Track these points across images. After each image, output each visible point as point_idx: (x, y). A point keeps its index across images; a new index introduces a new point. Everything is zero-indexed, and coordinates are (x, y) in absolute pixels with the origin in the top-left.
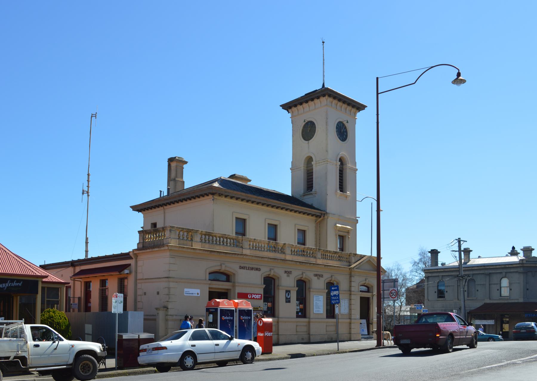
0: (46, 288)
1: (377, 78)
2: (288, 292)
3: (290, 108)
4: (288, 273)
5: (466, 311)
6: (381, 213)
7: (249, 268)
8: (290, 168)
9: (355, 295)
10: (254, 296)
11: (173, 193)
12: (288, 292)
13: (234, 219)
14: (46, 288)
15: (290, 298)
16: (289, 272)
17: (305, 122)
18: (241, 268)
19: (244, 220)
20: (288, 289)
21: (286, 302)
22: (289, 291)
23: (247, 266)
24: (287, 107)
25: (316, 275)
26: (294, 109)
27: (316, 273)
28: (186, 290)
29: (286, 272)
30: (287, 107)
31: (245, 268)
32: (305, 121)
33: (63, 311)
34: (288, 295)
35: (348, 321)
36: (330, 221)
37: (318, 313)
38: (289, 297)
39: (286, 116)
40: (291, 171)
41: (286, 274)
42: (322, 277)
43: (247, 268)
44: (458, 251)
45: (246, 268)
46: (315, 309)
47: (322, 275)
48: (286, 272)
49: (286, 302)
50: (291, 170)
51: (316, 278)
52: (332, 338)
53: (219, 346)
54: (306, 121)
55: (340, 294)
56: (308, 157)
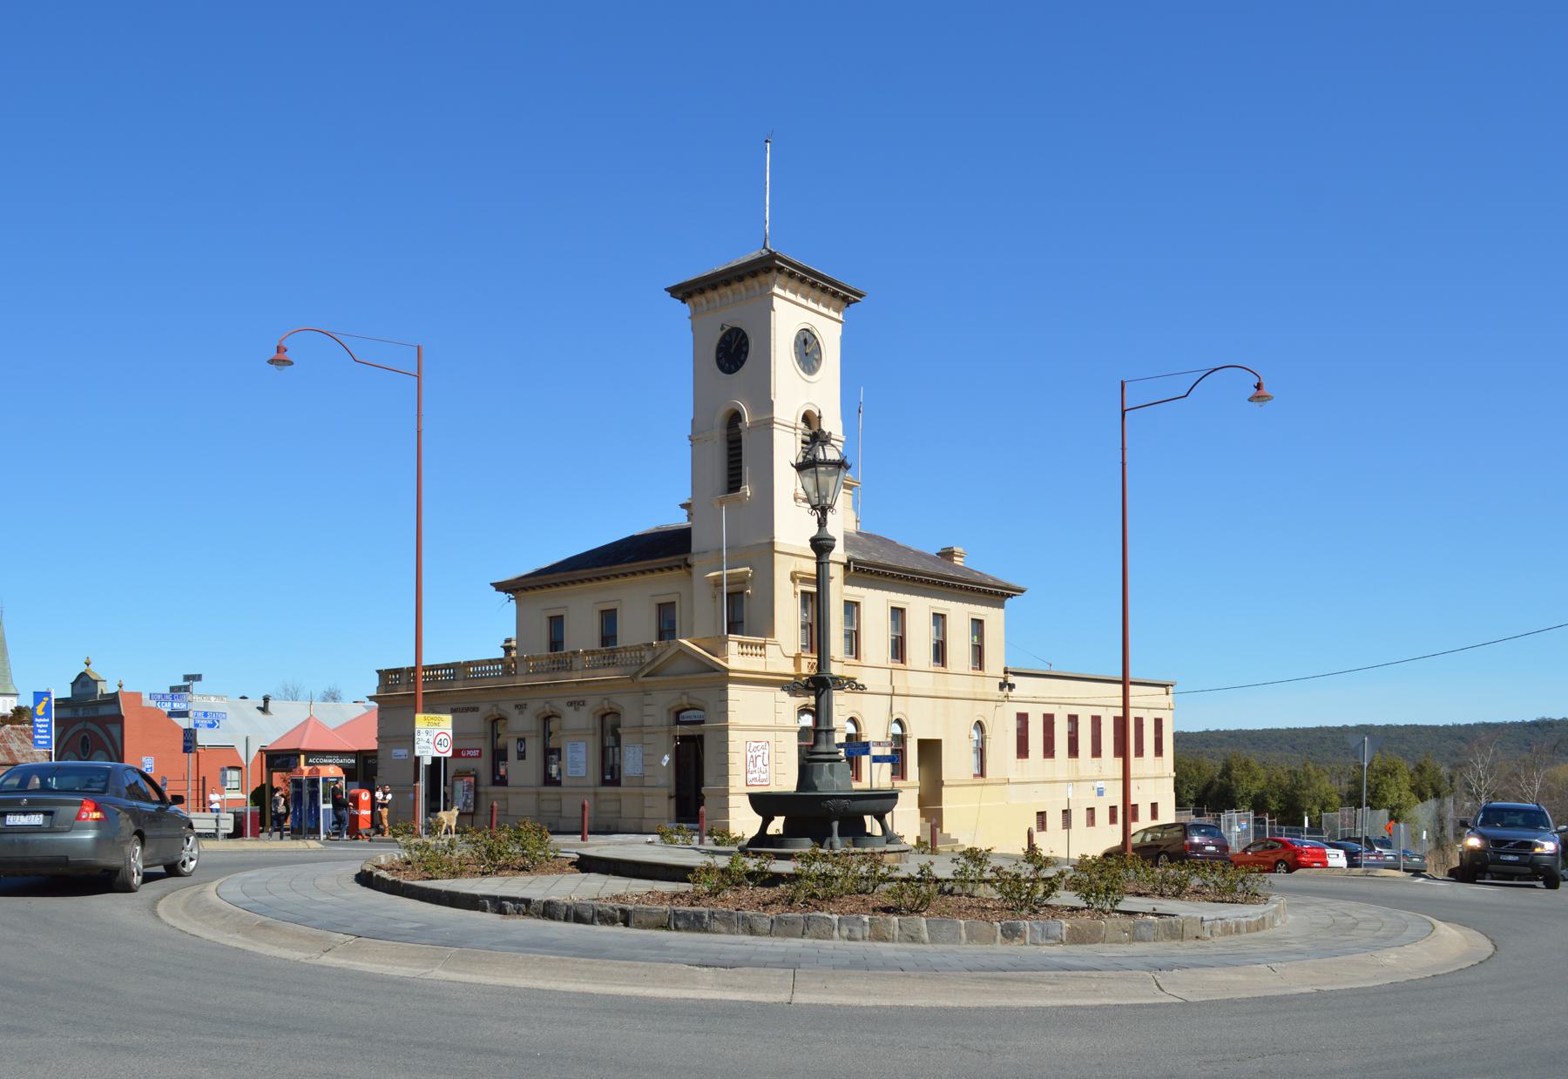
1: (1122, 382)
2: (521, 741)
4: (521, 707)
6: (1126, 452)
8: (690, 436)
9: (654, 733)
10: (469, 753)
11: (689, 673)
12: (521, 741)
13: (890, 609)
15: (524, 751)
17: (724, 331)
19: (902, 610)
20: (521, 736)
21: (519, 759)
23: (464, 705)
24: (683, 292)
25: (570, 704)
26: (698, 299)
27: (571, 699)
28: (394, 751)
29: (516, 706)
30: (683, 292)
32: (722, 329)
34: (521, 746)
35: (977, 805)
39: (683, 309)
40: (690, 442)
41: (517, 711)
46: (569, 769)
47: (583, 702)
48: (516, 706)
49: (519, 759)
50: (692, 441)
52: (609, 827)
53: (449, 708)
54: (727, 328)
56: (731, 410)
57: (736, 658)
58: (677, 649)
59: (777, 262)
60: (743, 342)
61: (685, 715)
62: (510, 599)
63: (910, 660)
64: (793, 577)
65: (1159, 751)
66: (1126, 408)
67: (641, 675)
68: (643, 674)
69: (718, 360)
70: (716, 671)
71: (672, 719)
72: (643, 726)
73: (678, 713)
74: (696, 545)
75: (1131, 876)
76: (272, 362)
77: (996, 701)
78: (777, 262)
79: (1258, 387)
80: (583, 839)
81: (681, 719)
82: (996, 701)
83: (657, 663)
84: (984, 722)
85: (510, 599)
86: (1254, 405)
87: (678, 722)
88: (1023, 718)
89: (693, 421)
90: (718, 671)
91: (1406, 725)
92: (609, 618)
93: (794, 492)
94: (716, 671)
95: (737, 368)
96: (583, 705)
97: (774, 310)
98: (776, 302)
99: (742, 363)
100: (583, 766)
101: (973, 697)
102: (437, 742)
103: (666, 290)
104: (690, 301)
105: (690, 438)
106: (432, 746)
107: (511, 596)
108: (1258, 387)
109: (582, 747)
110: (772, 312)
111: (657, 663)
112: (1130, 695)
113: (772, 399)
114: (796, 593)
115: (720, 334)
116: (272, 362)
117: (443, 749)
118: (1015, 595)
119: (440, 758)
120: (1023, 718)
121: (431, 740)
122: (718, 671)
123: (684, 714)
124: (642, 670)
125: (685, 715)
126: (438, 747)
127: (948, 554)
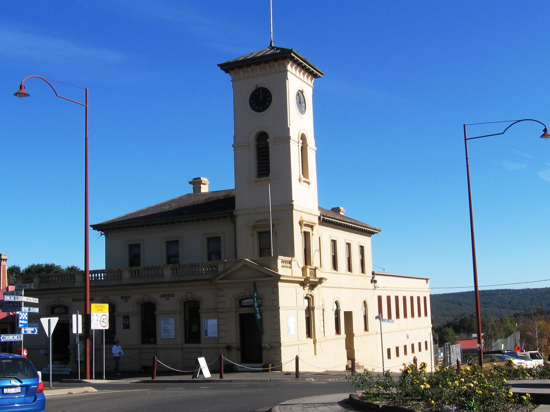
0: (23, 303)
1: (464, 125)
2: (126, 318)
3: (232, 69)
5: (384, 372)
7: (81, 300)
14: (23, 303)
16: (169, 295)
18: (74, 300)
22: (128, 317)
24: (227, 67)
27: (163, 293)
29: (122, 298)
30: (227, 67)
31: (77, 300)
33: (322, 218)
34: (126, 321)
36: (239, 220)
37: (167, 338)
38: (127, 323)
41: (123, 300)
42: (173, 297)
43: (80, 300)
44: (352, 367)
45: (78, 300)
51: (164, 299)
55: (292, 262)
57: (282, 271)
58: (243, 264)
59: (292, 54)
60: (267, 95)
61: (245, 302)
62: (102, 234)
63: (339, 268)
64: (300, 223)
65: (426, 315)
66: (467, 138)
67: (217, 279)
68: (219, 279)
69: (251, 104)
70: (272, 276)
71: (238, 305)
72: (218, 308)
73: (240, 301)
74: (239, 204)
75: (239, 369)
76: (16, 94)
77: (163, 283)
78: (292, 54)
79: (545, 130)
80: (221, 377)
81: (242, 304)
82: (163, 283)
83: (229, 272)
84: (367, 301)
85: (102, 234)
86: (543, 139)
87: (241, 306)
88: (380, 298)
89: (234, 137)
90: (218, 280)
91: (451, 293)
92: (172, 244)
93: (298, 178)
94: (272, 276)
95: (264, 110)
96: (173, 296)
97: (288, 79)
98: (289, 75)
99: (268, 107)
100: (173, 332)
101: (338, 286)
102: (102, 320)
103: (218, 65)
104: (232, 72)
105: (233, 146)
106: (99, 323)
107: (103, 233)
108: (545, 130)
109: (172, 321)
110: (287, 81)
111: (229, 272)
112: (478, 286)
113: (289, 126)
114: (301, 232)
115: (254, 89)
116: (16, 94)
117: (104, 325)
118: (377, 233)
119: (103, 330)
120: (380, 298)
121: (99, 320)
122: (218, 280)
123: (245, 301)
124: (218, 276)
125: (245, 302)
126: (102, 323)
127: (336, 210)
